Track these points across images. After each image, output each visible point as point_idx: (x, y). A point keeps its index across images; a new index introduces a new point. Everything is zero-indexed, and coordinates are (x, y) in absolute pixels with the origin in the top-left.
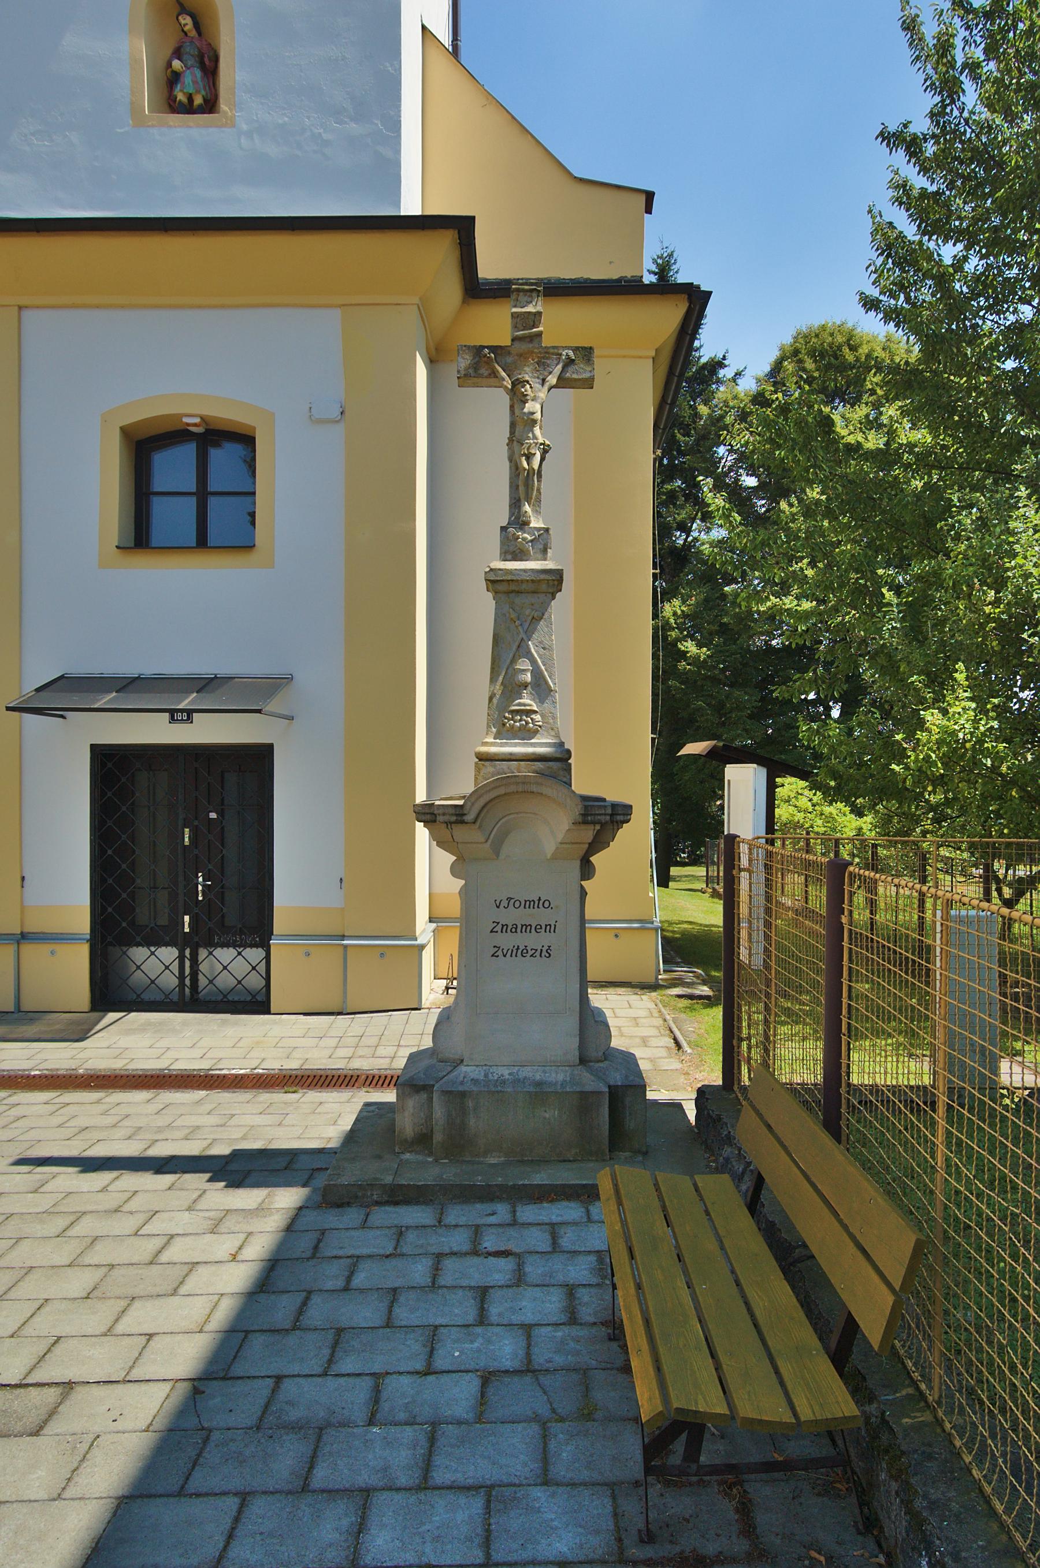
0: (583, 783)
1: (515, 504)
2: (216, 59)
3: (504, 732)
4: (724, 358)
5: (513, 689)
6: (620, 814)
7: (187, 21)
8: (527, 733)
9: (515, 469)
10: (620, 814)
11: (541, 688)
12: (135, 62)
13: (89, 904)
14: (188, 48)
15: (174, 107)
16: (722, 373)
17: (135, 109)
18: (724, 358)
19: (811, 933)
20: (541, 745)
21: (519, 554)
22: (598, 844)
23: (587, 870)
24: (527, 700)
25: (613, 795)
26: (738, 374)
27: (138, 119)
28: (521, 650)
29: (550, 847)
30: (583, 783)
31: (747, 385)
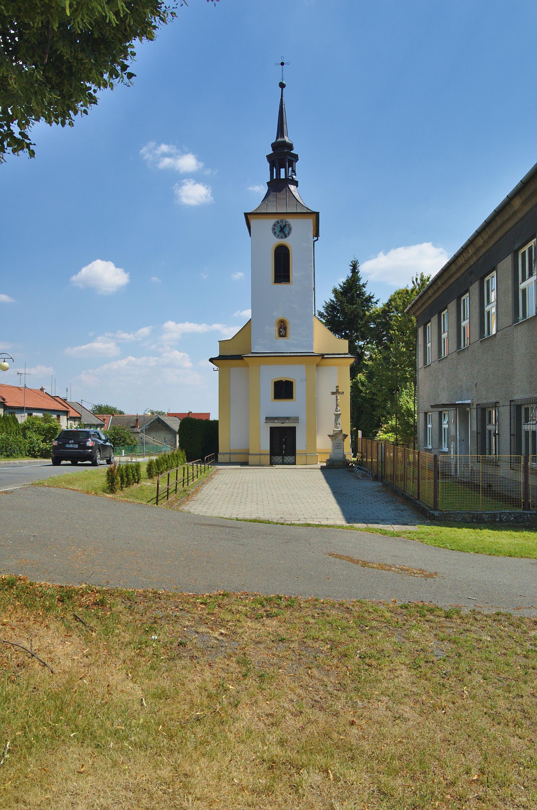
0: (344, 433)
1: (337, 407)
2: (286, 328)
3: (336, 428)
4: (373, 296)
5: (337, 424)
6: (347, 436)
7: (282, 324)
8: (338, 428)
9: (337, 404)
10: (347, 436)
11: (339, 424)
12: (276, 330)
13: (269, 449)
14: (283, 327)
15: (281, 336)
16: (372, 300)
17: (276, 337)
18: (373, 296)
19: (432, 461)
20: (339, 429)
21: (337, 412)
22: (345, 438)
23: (344, 441)
24: (338, 425)
25: (346, 434)
26: (378, 301)
27: (276, 338)
28: (338, 421)
29: (341, 439)
30: (344, 433)
31: (380, 306)
